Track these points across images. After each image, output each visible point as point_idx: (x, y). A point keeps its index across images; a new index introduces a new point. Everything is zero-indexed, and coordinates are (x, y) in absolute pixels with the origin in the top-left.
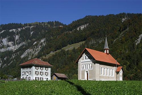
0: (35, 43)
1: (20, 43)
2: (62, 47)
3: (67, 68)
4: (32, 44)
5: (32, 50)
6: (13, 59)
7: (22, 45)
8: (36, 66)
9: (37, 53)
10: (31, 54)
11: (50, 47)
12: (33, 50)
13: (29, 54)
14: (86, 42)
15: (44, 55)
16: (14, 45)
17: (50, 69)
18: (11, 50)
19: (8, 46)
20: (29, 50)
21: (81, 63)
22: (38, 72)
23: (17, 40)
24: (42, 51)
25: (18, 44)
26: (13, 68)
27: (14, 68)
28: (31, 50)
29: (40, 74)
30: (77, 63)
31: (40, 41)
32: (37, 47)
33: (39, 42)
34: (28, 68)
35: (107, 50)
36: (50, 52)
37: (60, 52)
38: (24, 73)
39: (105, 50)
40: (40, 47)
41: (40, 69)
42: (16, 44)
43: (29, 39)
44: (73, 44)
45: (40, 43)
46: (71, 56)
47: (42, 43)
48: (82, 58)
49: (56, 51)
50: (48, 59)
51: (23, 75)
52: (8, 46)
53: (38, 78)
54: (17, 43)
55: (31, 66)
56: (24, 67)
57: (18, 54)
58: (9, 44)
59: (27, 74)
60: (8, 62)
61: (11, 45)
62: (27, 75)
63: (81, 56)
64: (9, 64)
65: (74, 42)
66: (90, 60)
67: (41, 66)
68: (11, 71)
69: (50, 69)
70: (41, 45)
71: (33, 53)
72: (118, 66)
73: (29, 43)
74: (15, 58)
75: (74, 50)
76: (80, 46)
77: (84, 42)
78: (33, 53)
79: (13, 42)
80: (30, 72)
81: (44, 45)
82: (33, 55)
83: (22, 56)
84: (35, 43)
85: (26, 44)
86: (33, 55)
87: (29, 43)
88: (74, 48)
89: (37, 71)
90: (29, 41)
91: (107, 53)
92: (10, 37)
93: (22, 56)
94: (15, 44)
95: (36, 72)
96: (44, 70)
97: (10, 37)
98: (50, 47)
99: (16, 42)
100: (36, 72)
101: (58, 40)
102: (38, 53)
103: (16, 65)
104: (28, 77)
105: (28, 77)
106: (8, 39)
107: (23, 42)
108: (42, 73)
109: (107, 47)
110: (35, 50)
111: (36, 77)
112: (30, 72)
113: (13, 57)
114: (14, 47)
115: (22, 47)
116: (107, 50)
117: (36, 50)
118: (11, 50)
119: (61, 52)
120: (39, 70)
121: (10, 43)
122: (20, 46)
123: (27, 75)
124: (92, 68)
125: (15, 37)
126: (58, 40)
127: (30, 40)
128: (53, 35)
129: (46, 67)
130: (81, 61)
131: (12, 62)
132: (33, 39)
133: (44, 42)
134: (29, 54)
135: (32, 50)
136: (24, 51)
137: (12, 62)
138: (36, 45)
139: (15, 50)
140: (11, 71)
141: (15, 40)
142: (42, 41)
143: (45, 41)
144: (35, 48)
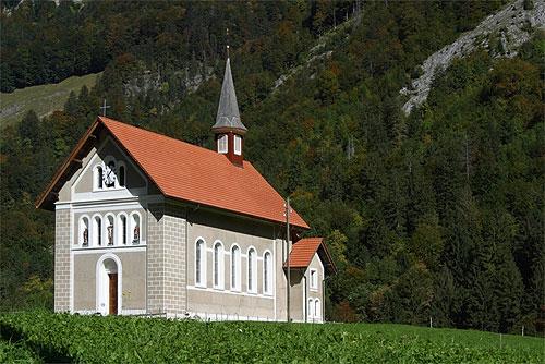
30: (50, 205)
39: (218, 136)
44: (21, 86)
48: (78, 177)
63: (76, 166)
65: (27, 75)
72: (295, 234)
76: (69, 106)
77: (91, 81)
88: (31, 114)
91: (230, 155)
109: (230, 117)
116: (231, 134)
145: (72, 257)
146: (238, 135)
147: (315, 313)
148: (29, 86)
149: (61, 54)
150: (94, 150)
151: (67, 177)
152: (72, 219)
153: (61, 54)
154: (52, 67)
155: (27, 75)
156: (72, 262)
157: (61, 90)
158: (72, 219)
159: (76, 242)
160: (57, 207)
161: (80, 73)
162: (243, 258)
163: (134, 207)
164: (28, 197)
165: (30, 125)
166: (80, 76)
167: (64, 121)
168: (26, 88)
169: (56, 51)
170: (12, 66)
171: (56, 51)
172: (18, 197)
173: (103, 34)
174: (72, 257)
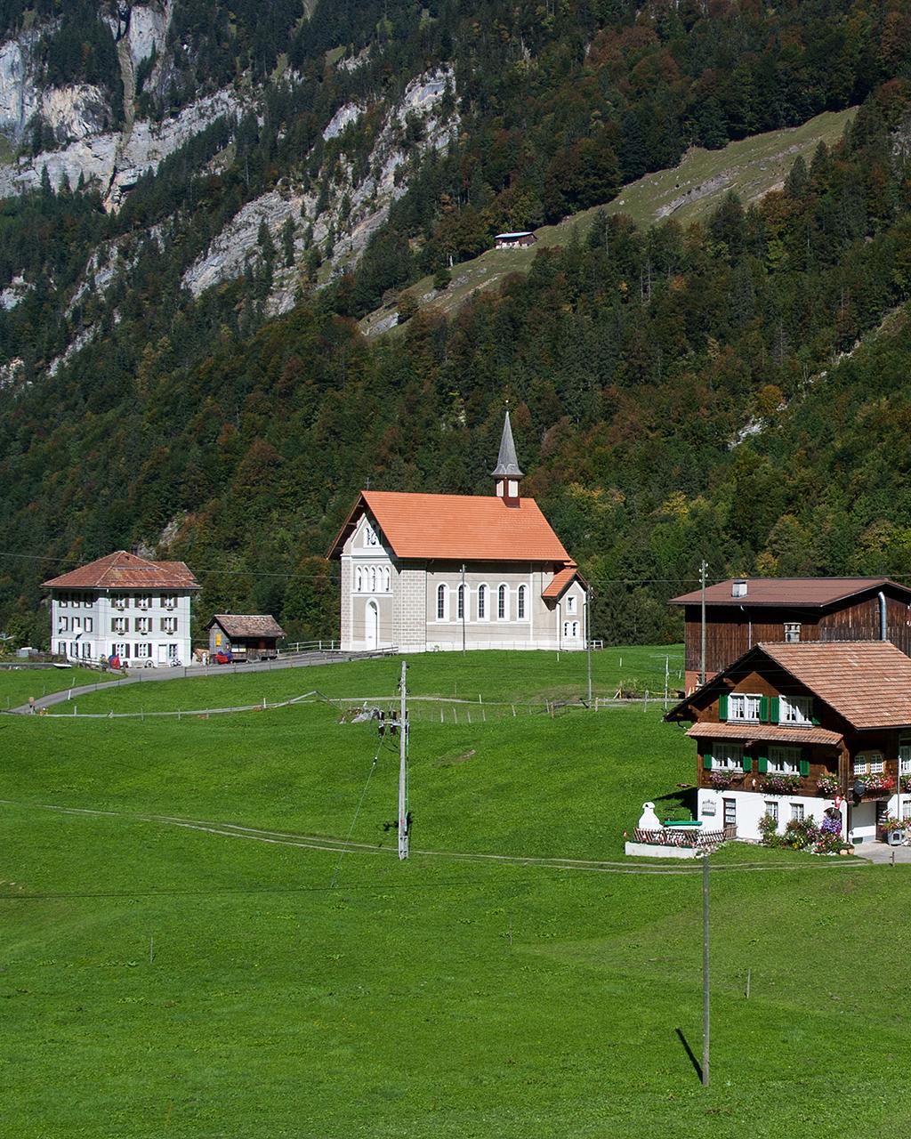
0: (349, 115)
1: (177, 103)
2: (619, 175)
3: (634, 428)
4: (313, 135)
5: (310, 202)
6: (94, 311)
7: (201, 126)
8: (115, 595)
9: (360, 233)
10: (299, 244)
11: (500, 180)
12: (322, 208)
13: (270, 254)
14: (860, 134)
15: (434, 267)
16: (111, 120)
17: (184, 602)
18: (74, 186)
19: (44, 138)
20: (273, 199)
21: (353, 562)
22: (127, 620)
23: (145, 70)
24: (411, 214)
25: (157, 111)
26: (102, 406)
27: (111, 415)
28: (296, 202)
29: (137, 629)
30: (337, 556)
31: (397, 99)
32: (362, 172)
33: (382, 113)
34: (82, 604)
35: (507, 479)
36: (494, 230)
37: (583, 240)
38: (64, 620)
39: (497, 480)
40: (389, 170)
41: (137, 605)
42: (140, 117)
43: (283, 58)
44: (738, 136)
45: (397, 127)
46: (691, 286)
47: (416, 129)
48: (355, 535)
49: (553, 220)
50: (457, 323)
51: (61, 631)
52: (44, 138)
53: (128, 646)
54: (143, 100)
55: (92, 594)
56: (65, 595)
57: (151, 248)
58: (47, 111)
59: (78, 630)
60: (46, 332)
61: (78, 129)
62: (79, 636)
63: (351, 529)
64: (49, 359)
65: (749, 116)
66: (385, 554)
67: (140, 594)
68: (74, 447)
69: (184, 602)
70: (405, 146)
71: (321, 233)
72: (557, 567)
73: (280, 109)
74: (116, 294)
75: (727, 222)
76: (793, 183)
77: (831, 129)
78: (321, 233)
79: (94, 93)
80: (88, 622)
81: (442, 144)
82: (315, 262)
83: (202, 277)
84: (349, 115)
85: (251, 118)
86: (315, 262)
87: (280, 109)
88: (733, 200)
89: (118, 614)
90: (287, 76)
91: (506, 498)
92: (54, 27)
93: (202, 277)
94: (120, 116)
95: (115, 621)
96: (156, 609)
97: (54, 27)
98: (500, 180)
99: (130, 91)
100: (115, 621)
101: (586, 95)
102: (374, 240)
103: (131, 369)
104: (80, 642)
105: (80, 642)
106: (43, 52)
107: (210, 92)
108: (144, 625)
109: (508, 464)
110: (347, 204)
111: (114, 646)
112: (88, 622)
113: (105, 277)
114: (107, 146)
115: (199, 148)
116: (507, 479)
117: (357, 197)
118: (74, 186)
119: (594, 242)
120: (132, 611)
121: (63, 105)
122: (188, 123)
123: (79, 636)
124: (391, 591)
125: (114, 26)
126: (586, 95)
127: (296, 63)
128: (536, 36)
129: (167, 594)
130: (351, 549)
131: (88, 336)
132: (332, 55)
133: (445, 107)
134: (270, 254)
135: (310, 202)
136: (216, 205)
137: (88, 336)
138: (357, 141)
139: (125, 179)
140: (74, 447)
141: (124, 62)
142: (422, 97)
143: (447, 102)
144: (340, 178)
145: (351, 599)
146: (513, 480)
147: (576, 641)
148: (752, 134)
149: (804, 74)
150: (364, 514)
151: (347, 535)
152: (352, 568)
153: (804, 74)
154: (790, 99)
155: (749, 116)
156: (351, 603)
157: (799, 142)
158: (352, 568)
159: (354, 588)
160: (343, 559)
161: (836, 106)
162: (511, 594)
163: (386, 562)
164: (716, 346)
165: (728, 220)
166: (837, 110)
167: (785, 207)
168: (749, 139)
169: (797, 69)
170: (724, 103)
171: (797, 69)
172: (700, 346)
173: (875, 33)
174: (351, 599)
